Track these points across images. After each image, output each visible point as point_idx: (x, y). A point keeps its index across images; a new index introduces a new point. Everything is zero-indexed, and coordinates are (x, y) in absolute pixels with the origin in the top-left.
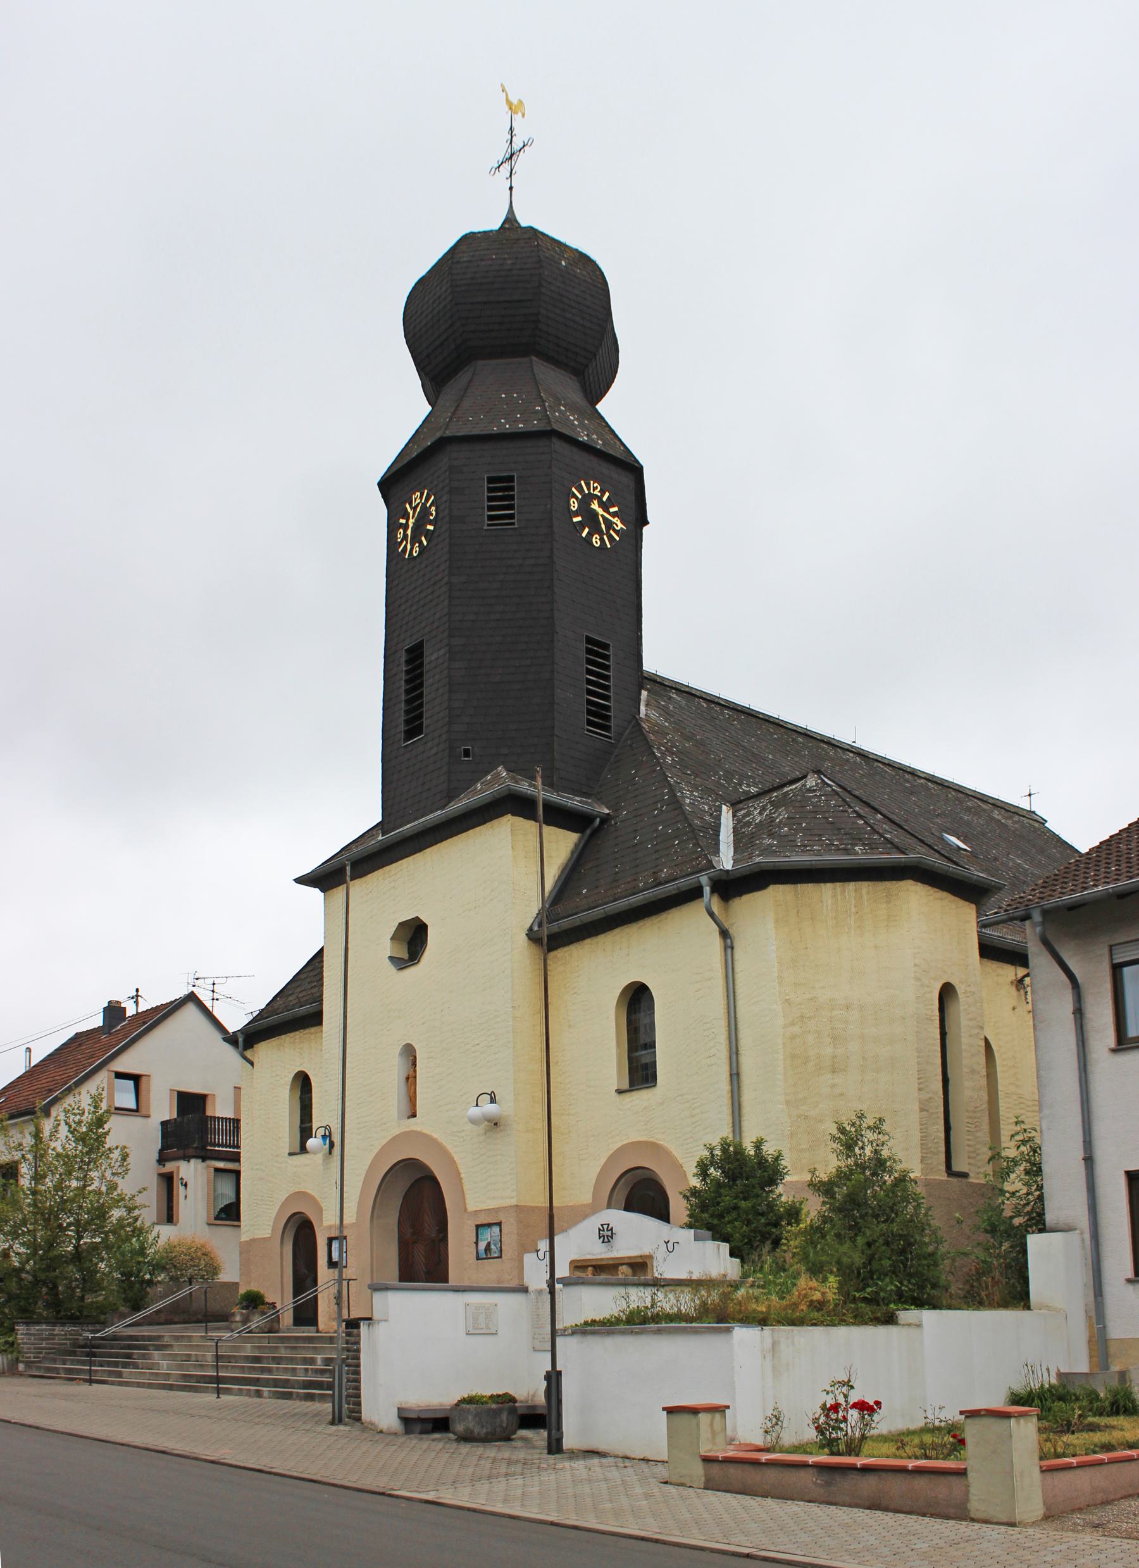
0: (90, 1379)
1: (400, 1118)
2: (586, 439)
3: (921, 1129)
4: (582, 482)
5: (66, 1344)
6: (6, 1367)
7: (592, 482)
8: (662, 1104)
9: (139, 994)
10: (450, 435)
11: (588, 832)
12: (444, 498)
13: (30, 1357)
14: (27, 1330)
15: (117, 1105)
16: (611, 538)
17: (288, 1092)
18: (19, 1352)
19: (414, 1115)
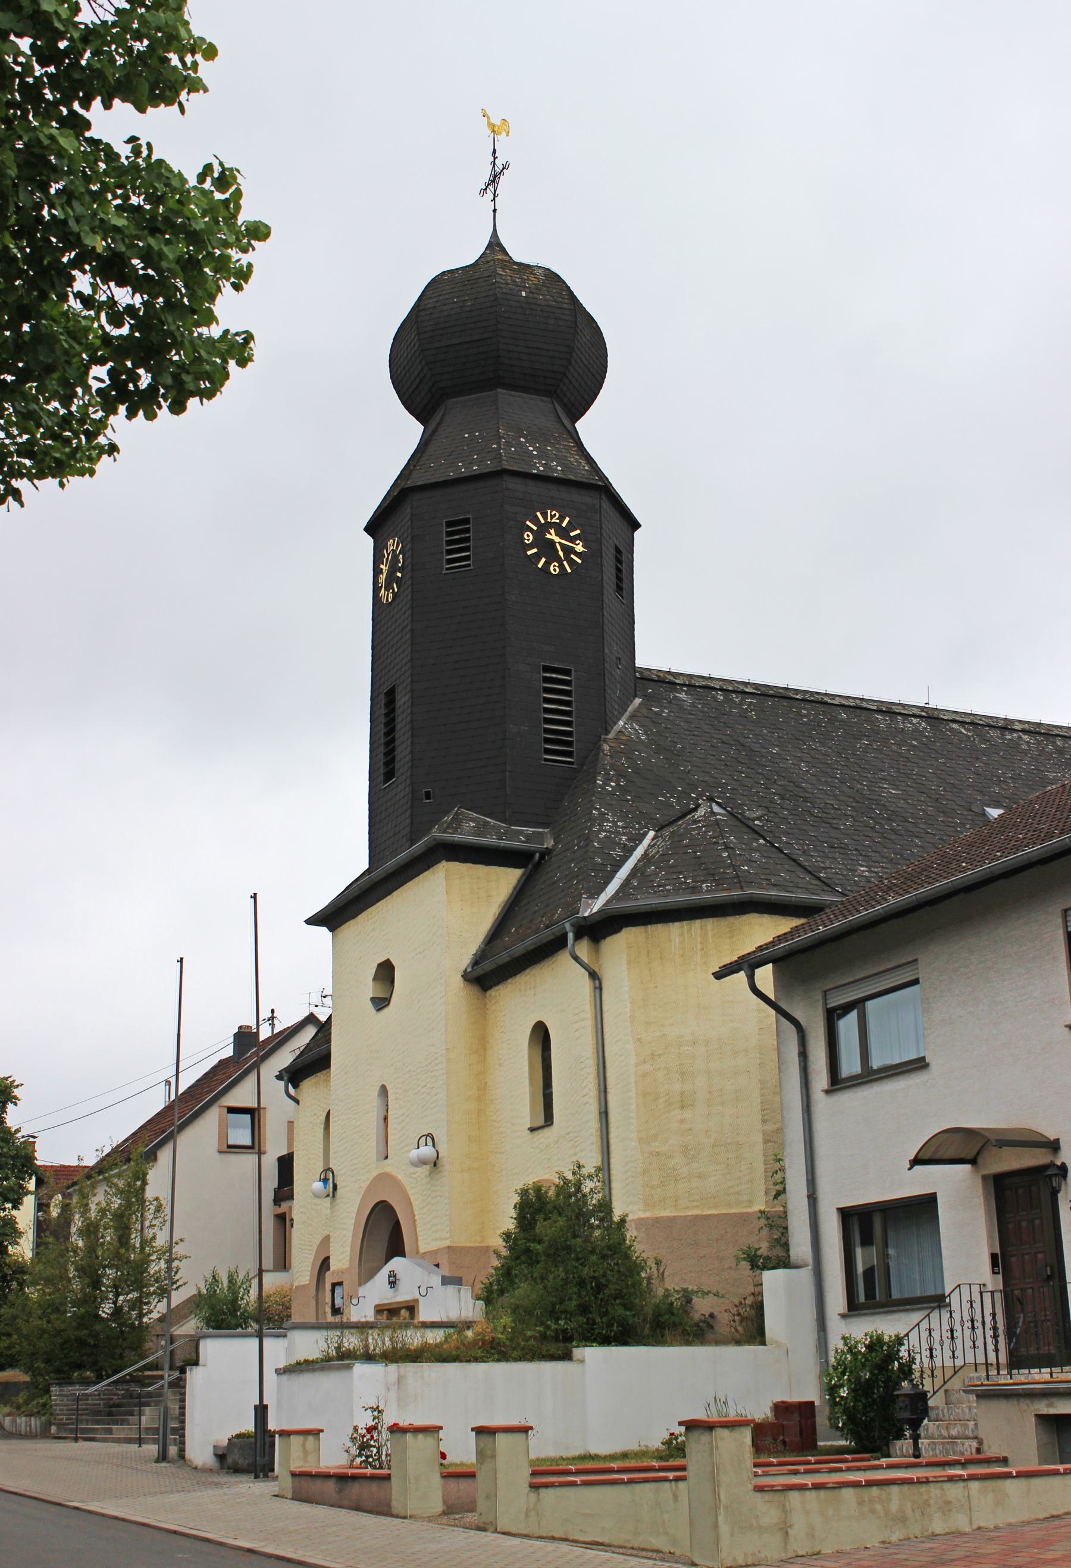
0: (140, 1438)
1: (378, 1160)
2: (542, 469)
3: (765, 1161)
4: (538, 514)
5: (99, 1404)
6: (39, 1429)
7: (549, 511)
8: (557, 1142)
9: (275, 1015)
10: (413, 485)
11: (530, 867)
12: (408, 546)
13: (62, 1419)
14: (60, 1391)
15: (230, 1143)
16: (572, 563)
17: (322, 1131)
18: (51, 1414)
19: (387, 1157)
